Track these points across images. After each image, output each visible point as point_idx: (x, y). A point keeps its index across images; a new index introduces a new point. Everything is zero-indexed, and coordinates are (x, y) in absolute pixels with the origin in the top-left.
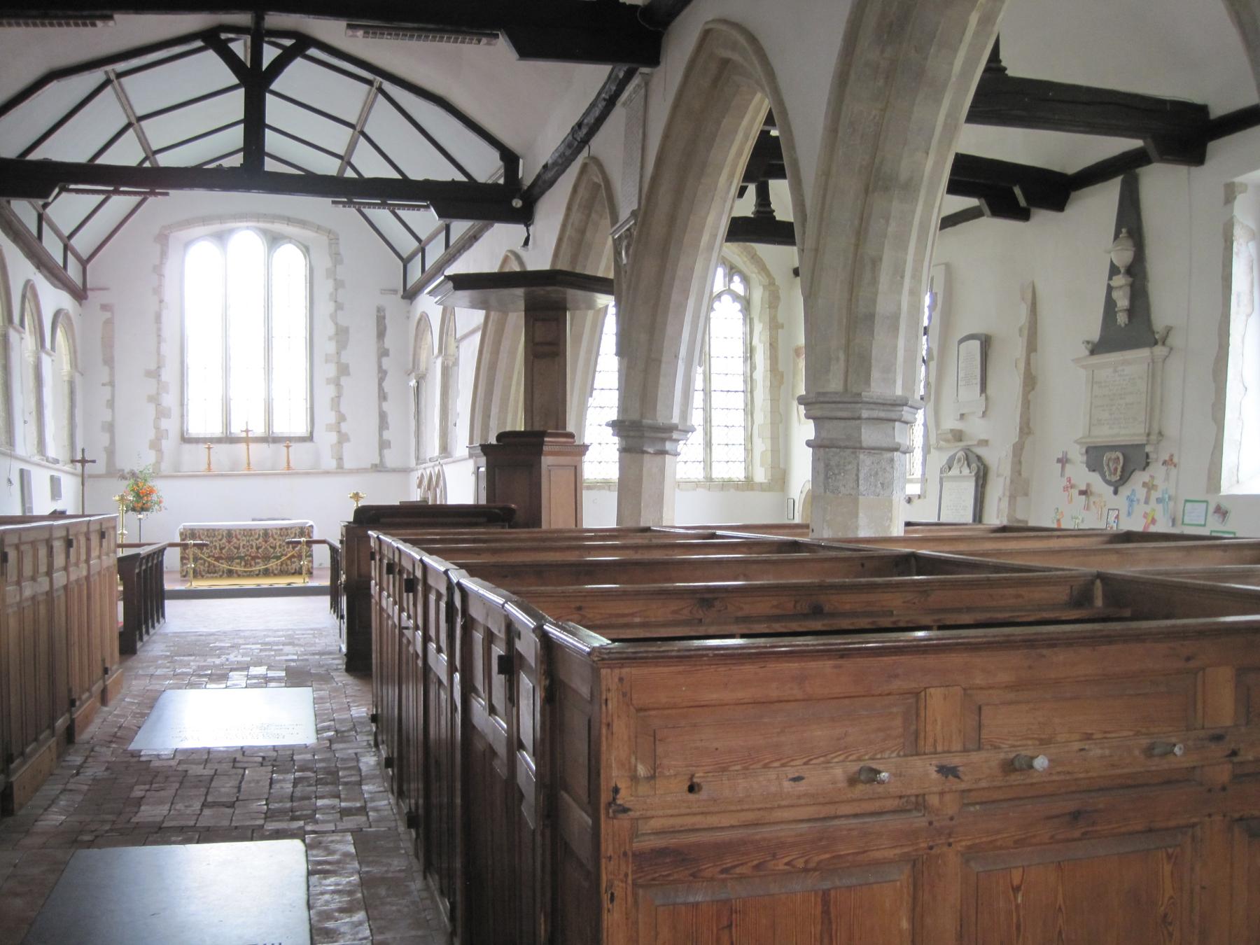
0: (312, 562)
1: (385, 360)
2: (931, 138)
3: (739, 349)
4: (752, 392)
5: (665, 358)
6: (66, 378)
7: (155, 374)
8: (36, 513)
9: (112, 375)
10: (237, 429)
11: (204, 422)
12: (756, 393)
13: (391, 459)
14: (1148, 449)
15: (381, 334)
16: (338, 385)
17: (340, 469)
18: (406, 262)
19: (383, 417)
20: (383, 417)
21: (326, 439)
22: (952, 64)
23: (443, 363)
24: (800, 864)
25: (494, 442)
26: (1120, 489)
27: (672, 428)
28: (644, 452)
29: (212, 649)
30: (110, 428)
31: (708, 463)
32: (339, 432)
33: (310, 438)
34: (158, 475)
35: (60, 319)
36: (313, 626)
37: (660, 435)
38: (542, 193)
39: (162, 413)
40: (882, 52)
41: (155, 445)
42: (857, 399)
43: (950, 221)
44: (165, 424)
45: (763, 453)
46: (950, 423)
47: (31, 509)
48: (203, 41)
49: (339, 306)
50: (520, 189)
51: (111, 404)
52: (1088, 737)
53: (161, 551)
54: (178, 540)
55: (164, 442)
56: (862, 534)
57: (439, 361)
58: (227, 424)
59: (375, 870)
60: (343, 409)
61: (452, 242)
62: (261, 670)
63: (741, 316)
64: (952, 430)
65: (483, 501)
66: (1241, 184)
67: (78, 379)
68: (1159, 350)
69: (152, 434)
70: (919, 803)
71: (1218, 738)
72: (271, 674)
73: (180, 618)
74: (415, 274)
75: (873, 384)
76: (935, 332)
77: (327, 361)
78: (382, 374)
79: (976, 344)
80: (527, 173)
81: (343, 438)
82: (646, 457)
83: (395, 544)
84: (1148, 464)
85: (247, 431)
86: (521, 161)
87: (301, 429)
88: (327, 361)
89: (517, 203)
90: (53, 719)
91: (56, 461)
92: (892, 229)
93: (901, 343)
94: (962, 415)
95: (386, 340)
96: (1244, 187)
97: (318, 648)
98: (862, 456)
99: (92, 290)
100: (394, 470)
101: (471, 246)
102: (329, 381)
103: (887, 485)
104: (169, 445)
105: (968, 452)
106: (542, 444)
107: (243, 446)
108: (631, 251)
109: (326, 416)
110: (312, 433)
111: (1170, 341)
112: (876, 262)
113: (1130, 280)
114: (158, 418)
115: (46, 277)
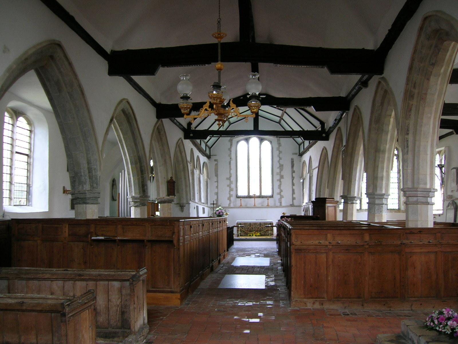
0: (273, 232)
1: (294, 174)
5: (353, 180)
6: (206, 180)
7: (229, 179)
8: (200, 216)
9: (217, 179)
10: (251, 194)
11: (242, 191)
15: (293, 166)
16: (280, 181)
17: (281, 206)
18: (300, 145)
20: (293, 191)
21: (277, 197)
23: (309, 175)
24: (313, 252)
25: (314, 200)
28: (348, 203)
29: (246, 251)
30: (217, 194)
32: (280, 195)
33: (272, 197)
34: (229, 207)
35: (205, 164)
36: (271, 247)
38: (330, 133)
39: (231, 190)
40: (376, 125)
43: (441, 138)
44: (232, 193)
46: (450, 193)
47: (199, 216)
49: (280, 159)
51: (217, 187)
53: (233, 228)
54: (236, 225)
55: (231, 198)
57: (308, 175)
59: (277, 278)
60: (282, 188)
61: (305, 148)
62: (259, 254)
64: (449, 195)
65: (312, 215)
67: (208, 180)
69: (228, 196)
71: (366, 242)
72: (260, 255)
73: (237, 245)
74: (302, 150)
75: (378, 191)
77: (277, 175)
78: (293, 178)
80: (327, 127)
82: (349, 204)
83: (285, 223)
86: (325, 124)
87: (270, 193)
88: (277, 175)
89: (324, 135)
90: (217, 258)
91: (204, 203)
92: (381, 159)
94: (452, 191)
97: (272, 251)
98: (376, 206)
99: (212, 156)
100: (296, 206)
101: (315, 144)
102: (278, 180)
104: (233, 199)
105: (453, 201)
106: (326, 201)
107: (253, 199)
109: (277, 191)
110: (273, 195)
112: (378, 166)
114: (230, 191)
115: (201, 154)
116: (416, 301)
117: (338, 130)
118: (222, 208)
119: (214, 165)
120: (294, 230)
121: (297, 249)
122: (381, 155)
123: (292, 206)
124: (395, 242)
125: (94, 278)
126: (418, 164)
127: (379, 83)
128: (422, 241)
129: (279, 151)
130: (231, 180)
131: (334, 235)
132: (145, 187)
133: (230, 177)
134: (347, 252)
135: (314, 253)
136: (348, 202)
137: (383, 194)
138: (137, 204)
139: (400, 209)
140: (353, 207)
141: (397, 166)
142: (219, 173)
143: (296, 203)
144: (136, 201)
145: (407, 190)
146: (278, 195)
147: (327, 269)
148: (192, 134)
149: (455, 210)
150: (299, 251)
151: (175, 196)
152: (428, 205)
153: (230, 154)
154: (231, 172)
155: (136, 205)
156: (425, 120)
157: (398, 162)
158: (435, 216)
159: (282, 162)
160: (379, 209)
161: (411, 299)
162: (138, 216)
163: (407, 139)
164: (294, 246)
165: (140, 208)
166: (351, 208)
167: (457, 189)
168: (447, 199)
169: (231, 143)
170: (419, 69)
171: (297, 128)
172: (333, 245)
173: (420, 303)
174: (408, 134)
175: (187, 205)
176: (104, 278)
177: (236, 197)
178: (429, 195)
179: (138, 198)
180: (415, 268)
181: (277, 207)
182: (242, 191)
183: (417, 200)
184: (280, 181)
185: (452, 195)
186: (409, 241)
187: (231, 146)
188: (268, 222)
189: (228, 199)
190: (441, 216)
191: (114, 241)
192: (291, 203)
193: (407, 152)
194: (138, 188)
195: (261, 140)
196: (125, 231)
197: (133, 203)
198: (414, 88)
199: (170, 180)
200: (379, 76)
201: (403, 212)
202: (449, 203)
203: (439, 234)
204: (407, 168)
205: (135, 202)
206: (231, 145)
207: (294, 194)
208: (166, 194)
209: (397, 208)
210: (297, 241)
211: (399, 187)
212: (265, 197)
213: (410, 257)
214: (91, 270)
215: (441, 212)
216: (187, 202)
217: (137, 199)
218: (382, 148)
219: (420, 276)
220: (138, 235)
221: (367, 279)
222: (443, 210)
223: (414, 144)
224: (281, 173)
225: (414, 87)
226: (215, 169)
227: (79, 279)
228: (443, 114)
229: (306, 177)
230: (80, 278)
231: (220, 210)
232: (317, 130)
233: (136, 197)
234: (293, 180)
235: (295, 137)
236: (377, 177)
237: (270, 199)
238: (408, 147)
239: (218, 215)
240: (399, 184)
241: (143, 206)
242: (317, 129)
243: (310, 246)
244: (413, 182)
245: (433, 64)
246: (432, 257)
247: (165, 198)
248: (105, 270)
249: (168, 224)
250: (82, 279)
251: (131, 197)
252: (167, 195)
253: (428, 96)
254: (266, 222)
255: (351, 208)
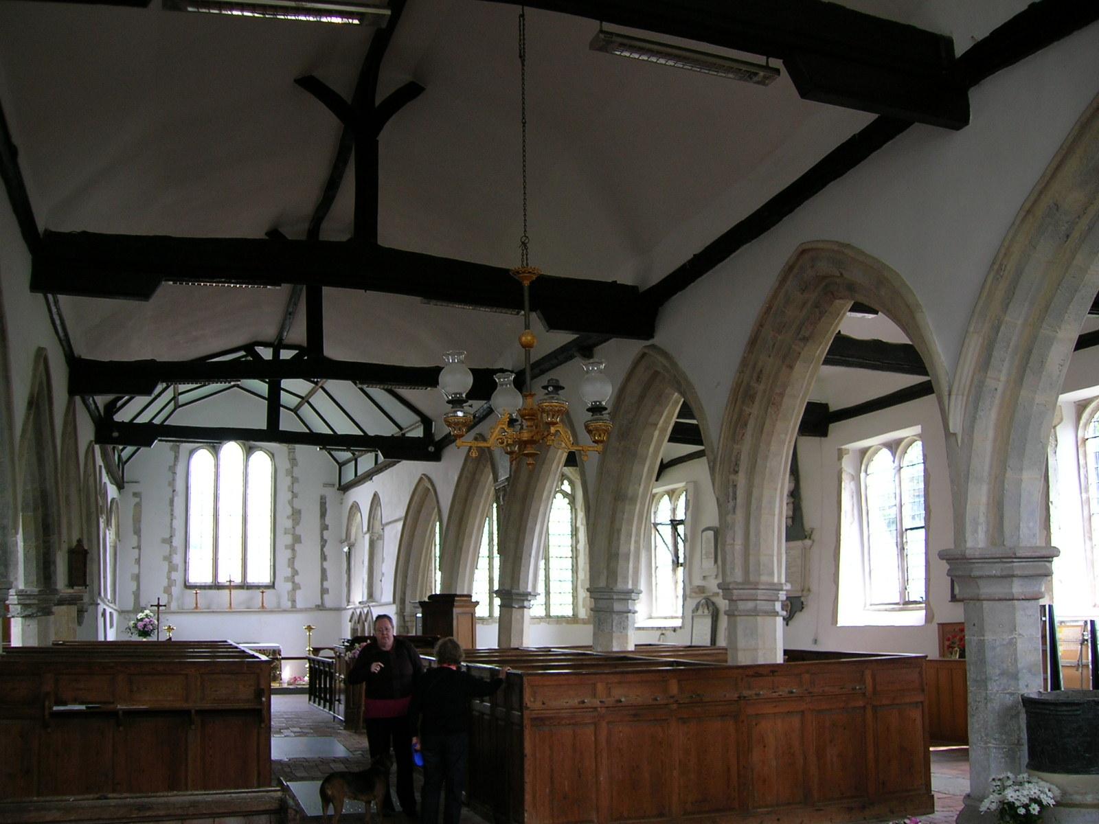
1: (325, 532)
2: (641, 478)
3: (568, 529)
4: (576, 558)
7: (169, 541)
9: (139, 541)
10: (222, 579)
11: (199, 573)
12: (579, 559)
13: (329, 602)
14: (802, 599)
15: (323, 514)
16: (293, 550)
17: (294, 609)
18: (341, 465)
19: (323, 571)
20: (323, 571)
21: (284, 587)
22: (648, 450)
23: (370, 538)
25: (427, 600)
26: (790, 623)
27: (529, 594)
30: (137, 578)
31: (547, 605)
32: (293, 582)
33: (272, 586)
37: (522, 598)
39: (173, 568)
41: (167, 590)
42: (611, 591)
44: (174, 575)
45: (584, 599)
46: (698, 582)
48: (245, 351)
49: (295, 495)
50: (433, 440)
51: (138, 561)
52: (638, 696)
56: (615, 649)
57: (367, 537)
58: (215, 575)
60: (297, 566)
63: (569, 507)
64: (698, 586)
66: (846, 449)
68: (808, 542)
69: (165, 582)
70: (595, 708)
71: (672, 697)
74: (349, 475)
75: (618, 584)
76: (688, 522)
77: (285, 533)
78: (324, 542)
79: (711, 533)
81: (296, 587)
84: (803, 608)
85: (230, 581)
87: (265, 579)
89: (431, 449)
92: (626, 516)
93: (631, 565)
94: (704, 577)
95: (326, 518)
96: (847, 451)
98: (614, 616)
100: (331, 609)
102: (287, 547)
103: (625, 628)
104: (176, 590)
105: (707, 599)
106: (454, 601)
107: (227, 591)
108: (506, 498)
110: (274, 583)
111: (813, 537)
112: (619, 531)
113: (792, 500)
114: (170, 572)
116: (768, 813)
117: (118, 397)
118: (152, 614)
119: (132, 507)
120: (529, 678)
121: (536, 719)
122: (627, 507)
123: (321, 610)
124: (727, 695)
125: (180, 812)
126: (758, 534)
127: (643, 355)
128: (776, 690)
129: (292, 477)
130: (174, 544)
131: (609, 686)
132: (52, 568)
133: (171, 536)
134: (635, 719)
135: (569, 724)
136: (514, 605)
137: (630, 589)
138: (30, 610)
139: (577, 615)
140: (522, 617)
141: (570, 521)
142: (143, 526)
143: (329, 601)
144: (28, 602)
145: (737, 587)
146: (287, 581)
147: (596, 758)
148: (118, 432)
149: (712, 618)
150: (539, 721)
151: (86, 588)
152: (776, 616)
153: (174, 480)
154: (173, 524)
155: (26, 613)
156: (773, 448)
157: (574, 510)
158: (664, 632)
159: (297, 505)
160: (621, 623)
161: (759, 810)
162: (33, 643)
163: (733, 482)
164: (528, 712)
165: (36, 621)
166: (519, 617)
167: (715, 573)
168: (693, 595)
169: (175, 452)
170: (774, 345)
171: (344, 427)
172: (607, 707)
173: (777, 818)
174: (737, 472)
175: (91, 608)
176: (204, 812)
177: (183, 586)
178: (779, 597)
179: (34, 595)
180: (765, 747)
181: (285, 611)
182: (199, 573)
183: (756, 607)
184: (293, 550)
185: (704, 587)
186: (754, 692)
187: (175, 461)
188: (269, 648)
189: (165, 592)
190: (679, 631)
191: (115, 713)
192: (319, 602)
193: (734, 508)
194: (34, 570)
195: (249, 451)
196: (135, 689)
197: (19, 607)
198: (758, 381)
199: (77, 545)
200: (643, 341)
201: (584, 622)
202: (699, 603)
203: (807, 676)
204: (732, 542)
205: (25, 606)
206: (176, 458)
207: (327, 580)
208: (66, 582)
209: (570, 613)
210: (534, 701)
211: (575, 567)
212: (253, 586)
213: (756, 725)
214: (169, 794)
215: (678, 623)
216: (91, 602)
217: (32, 597)
218: (630, 492)
219: (774, 763)
220: (169, 699)
221: (675, 773)
222: (683, 617)
223: (749, 494)
224: (295, 530)
225: (758, 380)
226: (133, 516)
227: (140, 817)
228: (678, 418)
229: (355, 540)
230: (141, 814)
231: (147, 619)
232: (404, 434)
233: (28, 593)
234: (323, 547)
235: (333, 449)
236: (618, 554)
237: (268, 592)
238: (735, 498)
239: (142, 629)
240: (575, 560)
241: (44, 615)
242: (403, 432)
243: (563, 711)
244: (746, 572)
245: (805, 340)
246: (796, 721)
247: (63, 591)
248: (206, 792)
249: (245, 668)
250: (148, 816)
251: (16, 592)
252: (67, 586)
253: (786, 399)
254: (265, 648)
255: (519, 617)
